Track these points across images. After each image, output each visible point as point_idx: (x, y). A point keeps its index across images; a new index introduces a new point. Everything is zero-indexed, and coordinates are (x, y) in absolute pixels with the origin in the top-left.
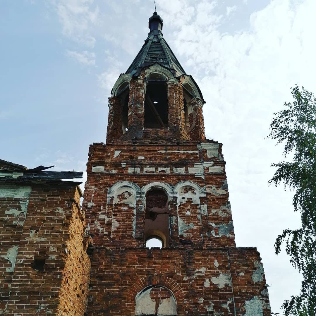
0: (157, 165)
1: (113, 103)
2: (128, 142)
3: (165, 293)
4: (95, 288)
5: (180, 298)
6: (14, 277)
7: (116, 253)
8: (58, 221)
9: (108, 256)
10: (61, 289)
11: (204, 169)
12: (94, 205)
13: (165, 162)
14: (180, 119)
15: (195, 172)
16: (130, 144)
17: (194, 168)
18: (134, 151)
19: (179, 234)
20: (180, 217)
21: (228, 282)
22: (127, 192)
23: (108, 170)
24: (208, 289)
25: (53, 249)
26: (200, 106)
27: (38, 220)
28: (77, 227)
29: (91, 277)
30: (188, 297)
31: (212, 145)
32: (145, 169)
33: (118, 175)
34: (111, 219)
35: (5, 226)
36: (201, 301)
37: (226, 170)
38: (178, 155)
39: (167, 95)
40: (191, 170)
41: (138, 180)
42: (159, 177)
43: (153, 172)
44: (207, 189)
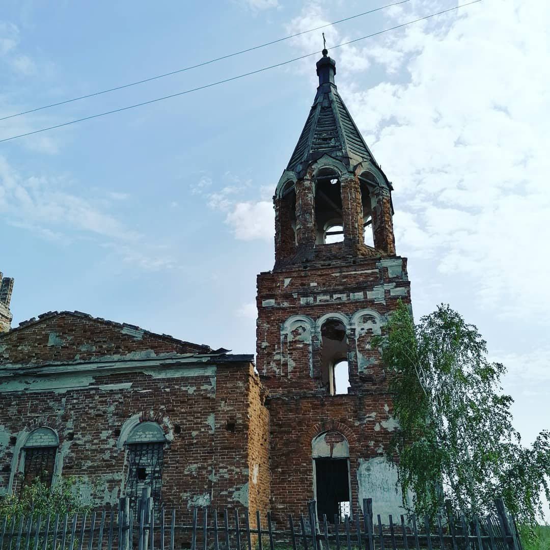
0: (332, 292)
1: (278, 208)
2: (298, 267)
3: (339, 437)
4: (276, 435)
5: (351, 442)
6: (215, 438)
7: (292, 402)
8: (240, 393)
9: (285, 405)
10: (248, 444)
11: (385, 293)
12: (268, 344)
13: (341, 287)
14: (357, 226)
15: (374, 297)
16: (300, 269)
17: (373, 292)
18: (305, 277)
19: (359, 371)
20: (359, 351)
21: (398, 425)
22: (301, 326)
23: (279, 304)
24: (378, 433)
25: (239, 416)
26: (385, 198)
27: (225, 393)
28: (254, 392)
29: (271, 426)
30: (359, 441)
31: (394, 261)
32: (319, 298)
33: (290, 308)
34: (286, 358)
35: (202, 399)
36: (372, 443)
37: (411, 292)
38: (355, 277)
39: (340, 196)
40: (370, 295)
41: (312, 311)
42: (335, 306)
43: (328, 301)
44: (388, 317)
